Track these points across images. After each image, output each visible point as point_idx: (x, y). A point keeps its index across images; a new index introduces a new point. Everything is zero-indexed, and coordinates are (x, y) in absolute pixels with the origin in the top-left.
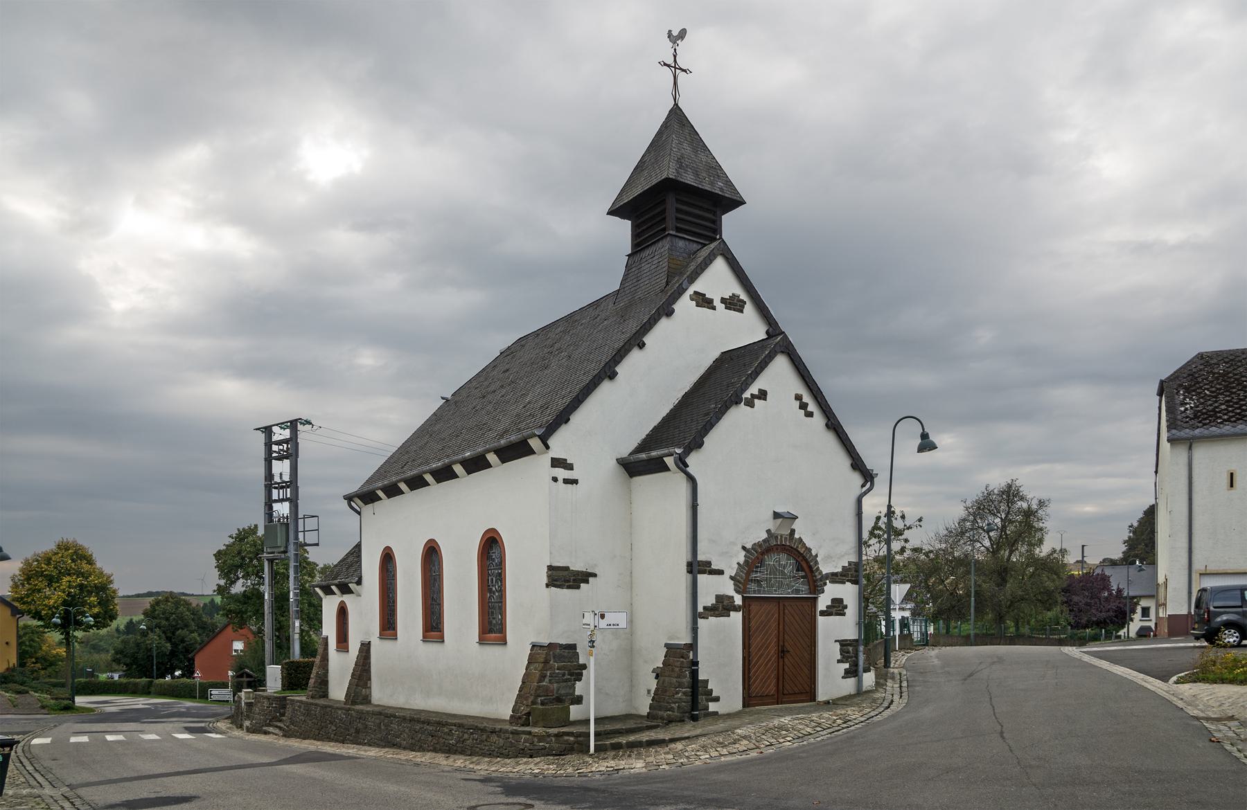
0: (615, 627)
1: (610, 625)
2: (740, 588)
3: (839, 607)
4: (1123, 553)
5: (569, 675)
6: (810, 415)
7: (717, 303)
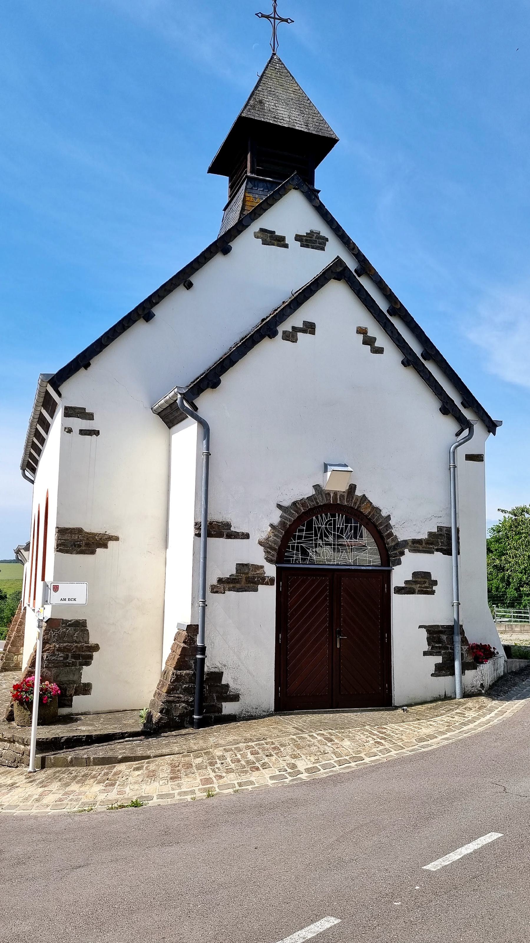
0: (70, 602)
1: (65, 600)
3: (425, 582)
4: (256, 590)
5: (72, 657)
6: (379, 351)
7: (290, 240)
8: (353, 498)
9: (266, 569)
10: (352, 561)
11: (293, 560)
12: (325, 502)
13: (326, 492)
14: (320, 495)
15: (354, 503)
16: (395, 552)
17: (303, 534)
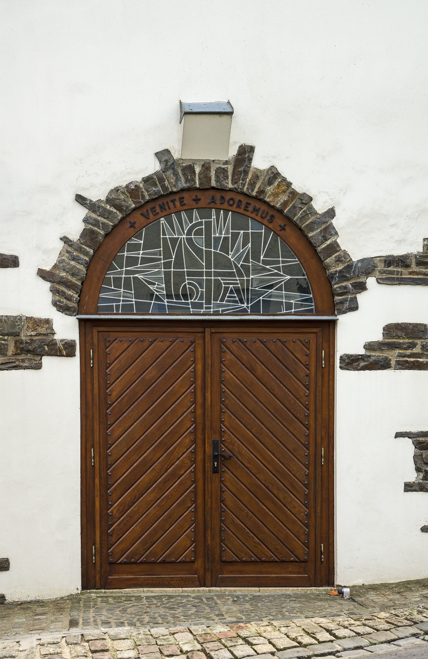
2: (69, 298)
3: (413, 345)
4: (38, 367)
8: (246, 172)
9: (56, 327)
10: (250, 305)
11: (118, 307)
12: (181, 184)
13: (184, 165)
14: (170, 173)
15: (250, 184)
16: (344, 284)
17: (139, 254)
